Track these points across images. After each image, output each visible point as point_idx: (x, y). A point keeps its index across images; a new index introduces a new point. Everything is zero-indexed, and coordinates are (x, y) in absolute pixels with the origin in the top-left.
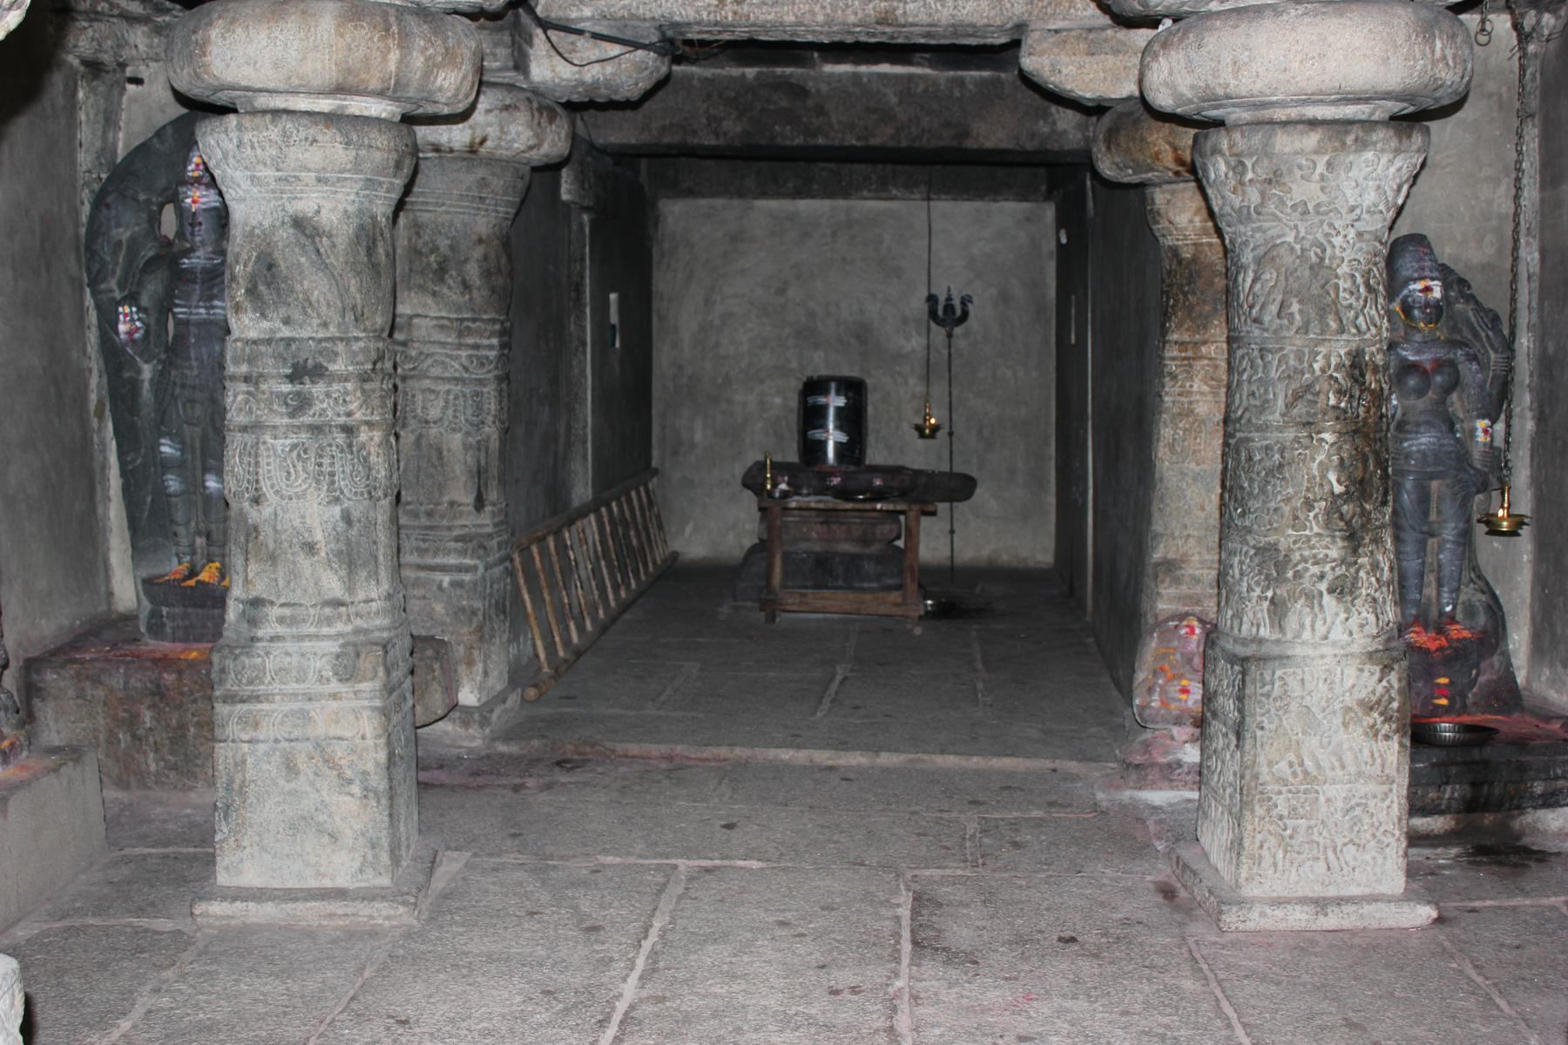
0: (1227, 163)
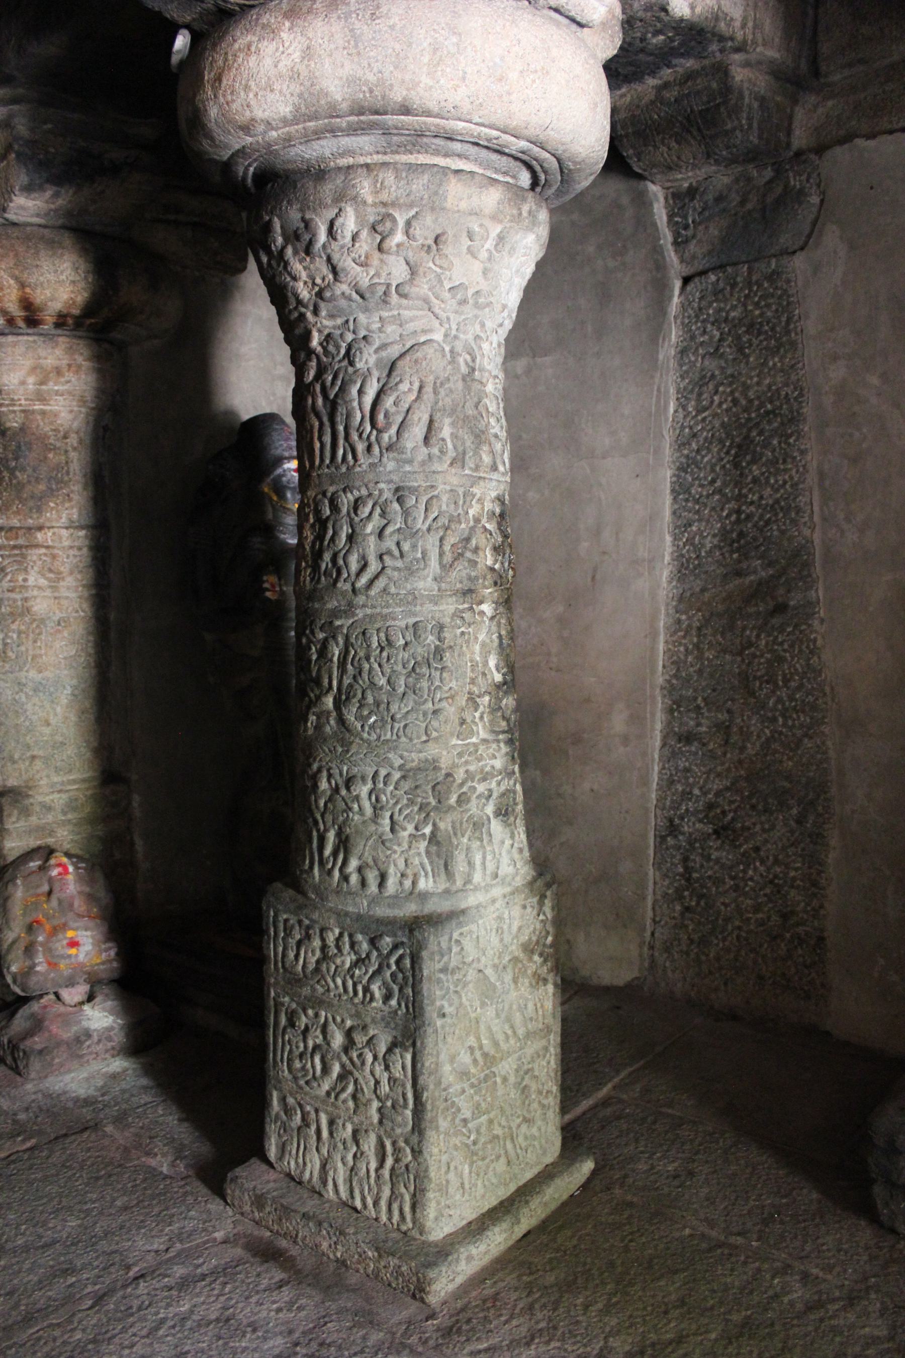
0: (360, 219)
